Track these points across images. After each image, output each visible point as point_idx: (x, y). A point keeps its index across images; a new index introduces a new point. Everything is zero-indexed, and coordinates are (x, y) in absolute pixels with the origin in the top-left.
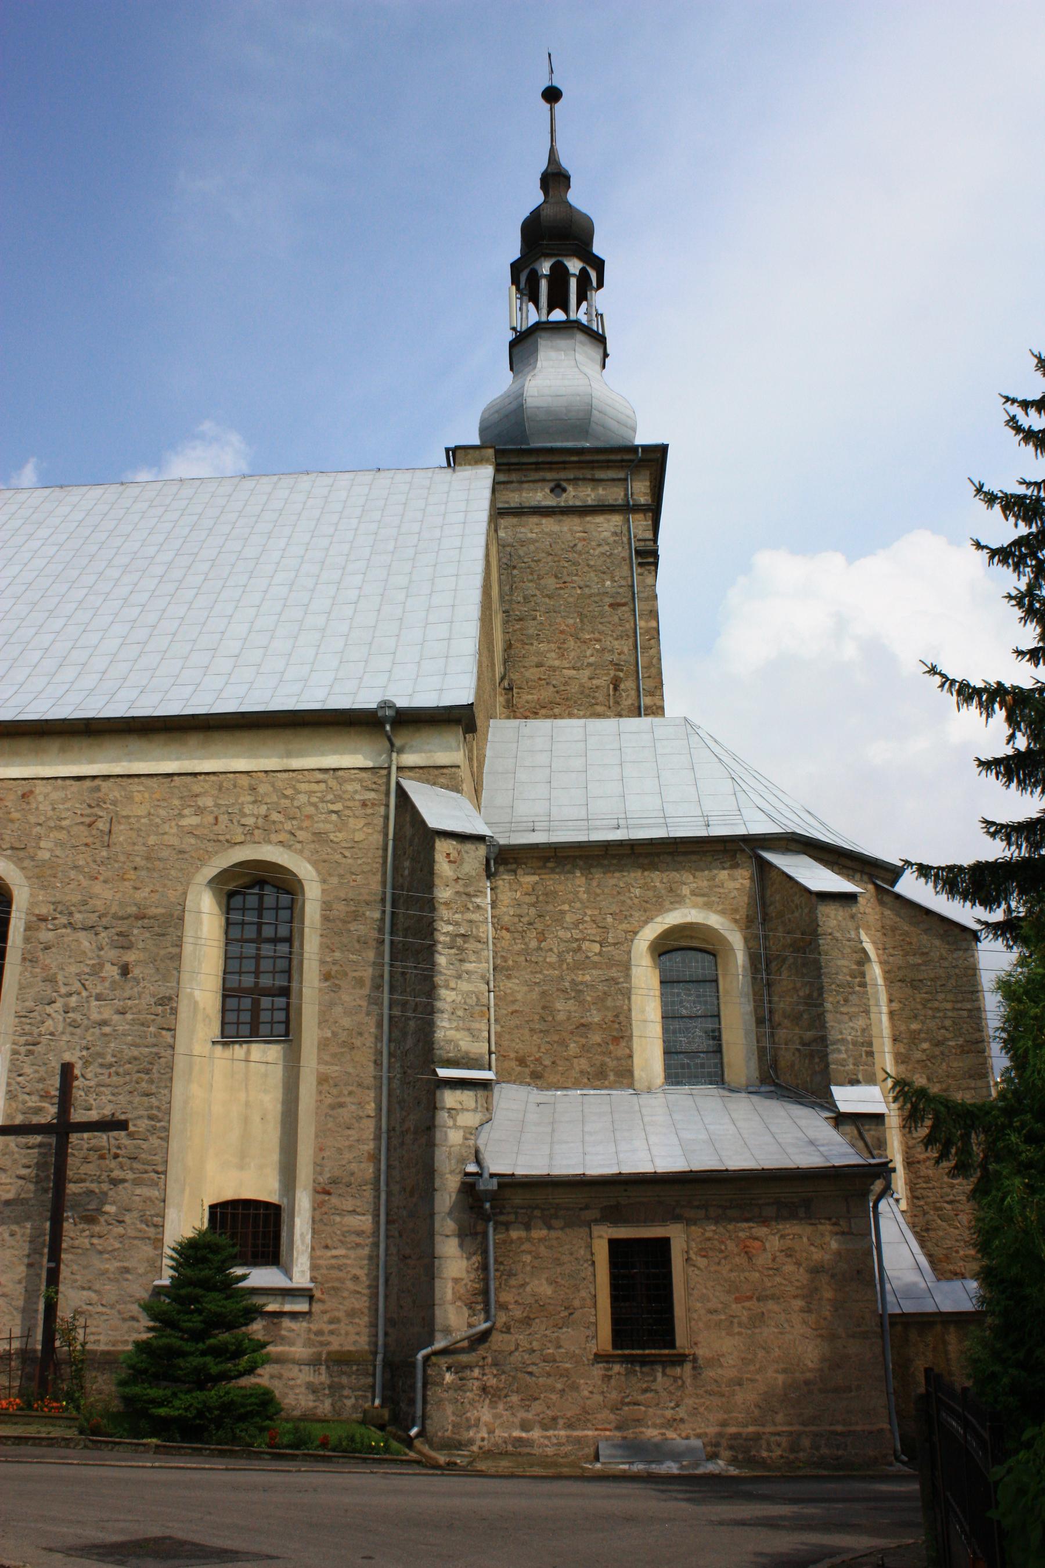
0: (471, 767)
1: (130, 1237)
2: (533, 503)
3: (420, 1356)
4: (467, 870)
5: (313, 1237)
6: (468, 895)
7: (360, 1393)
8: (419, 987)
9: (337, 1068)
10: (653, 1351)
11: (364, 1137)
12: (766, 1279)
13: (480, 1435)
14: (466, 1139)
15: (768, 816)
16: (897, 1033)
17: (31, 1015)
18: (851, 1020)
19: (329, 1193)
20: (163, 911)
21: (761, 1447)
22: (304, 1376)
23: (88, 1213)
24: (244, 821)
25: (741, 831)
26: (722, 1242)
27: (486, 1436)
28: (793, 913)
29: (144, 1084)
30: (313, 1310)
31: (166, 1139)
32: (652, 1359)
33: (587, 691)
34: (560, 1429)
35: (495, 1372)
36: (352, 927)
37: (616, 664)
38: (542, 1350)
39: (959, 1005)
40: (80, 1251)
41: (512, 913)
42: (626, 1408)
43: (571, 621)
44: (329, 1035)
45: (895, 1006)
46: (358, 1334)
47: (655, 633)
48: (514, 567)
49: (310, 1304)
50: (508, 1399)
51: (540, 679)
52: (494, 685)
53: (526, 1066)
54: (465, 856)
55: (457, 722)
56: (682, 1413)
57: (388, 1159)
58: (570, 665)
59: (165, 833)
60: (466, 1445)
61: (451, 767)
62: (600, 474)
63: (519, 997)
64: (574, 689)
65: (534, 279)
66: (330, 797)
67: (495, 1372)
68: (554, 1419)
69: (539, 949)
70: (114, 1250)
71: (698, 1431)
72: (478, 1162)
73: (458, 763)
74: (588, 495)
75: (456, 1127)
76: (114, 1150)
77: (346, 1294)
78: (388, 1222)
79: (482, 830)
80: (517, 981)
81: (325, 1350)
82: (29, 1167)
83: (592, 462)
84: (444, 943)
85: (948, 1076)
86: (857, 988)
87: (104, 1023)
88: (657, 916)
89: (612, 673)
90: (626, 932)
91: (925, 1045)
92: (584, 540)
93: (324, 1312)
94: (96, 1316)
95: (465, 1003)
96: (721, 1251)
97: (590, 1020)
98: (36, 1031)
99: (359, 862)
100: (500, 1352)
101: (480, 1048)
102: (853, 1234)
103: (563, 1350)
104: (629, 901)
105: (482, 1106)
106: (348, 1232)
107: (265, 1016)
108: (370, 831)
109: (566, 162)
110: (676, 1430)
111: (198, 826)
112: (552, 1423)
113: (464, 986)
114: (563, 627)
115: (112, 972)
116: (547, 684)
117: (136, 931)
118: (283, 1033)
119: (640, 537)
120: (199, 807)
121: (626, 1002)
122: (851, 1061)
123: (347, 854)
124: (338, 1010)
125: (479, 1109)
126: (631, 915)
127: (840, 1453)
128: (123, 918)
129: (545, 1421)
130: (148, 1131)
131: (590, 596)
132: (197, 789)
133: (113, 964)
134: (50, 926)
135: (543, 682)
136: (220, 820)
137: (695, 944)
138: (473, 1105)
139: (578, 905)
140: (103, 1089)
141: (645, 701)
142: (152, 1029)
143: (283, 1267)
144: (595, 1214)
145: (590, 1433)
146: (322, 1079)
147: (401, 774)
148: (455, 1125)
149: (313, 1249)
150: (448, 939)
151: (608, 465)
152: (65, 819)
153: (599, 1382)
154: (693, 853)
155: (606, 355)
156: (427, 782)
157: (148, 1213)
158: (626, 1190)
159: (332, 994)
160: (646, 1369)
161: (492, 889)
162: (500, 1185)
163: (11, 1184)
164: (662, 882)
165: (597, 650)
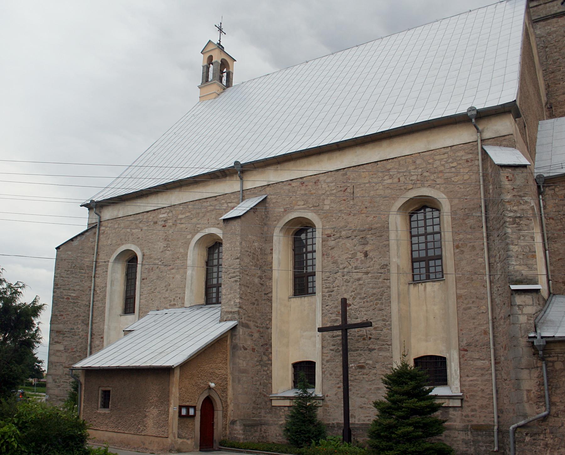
1: (379, 374)
2: (553, 13)
3: (511, 428)
5: (460, 372)
6: (520, 196)
7: (488, 444)
8: (500, 246)
9: (466, 290)
11: (482, 323)
17: (329, 279)
19: (466, 351)
20: (380, 225)
22: (461, 436)
23: (360, 364)
24: (412, 178)
29: (379, 305)
30: (463, 406)
31: (391, 329)
35: (552, 437)
36: (467, 222)
40: (358, 381)
41: (554, 210)
46: (485, 417)
48: (547, 47)
49: (462, 403)
52: (542, 105)
54: (516, 176)
55: (509, 112)
59: (377, 189)
61: (508, 135)
63: (561, 252)
66: (450, 160)
67: (552, 437)
70: (373, 380)
76: (369, 336)
78: (496, 363)
80: (560, 244)
81: (470, 424)
82: (335, 345)
84: (509, 222)
87: (359, 279)
93: (469, 406)
94: (368, 409)
95: (523, 251)
98: (332, 286)
99: (468, 189)
100: (553, 427)
106: (477, 368)
107: (432, 270)
108: (471, 174)
115: (360, 256)
117: (368, 236)
118: (441, 277)
123: (462, 187)
124: (464, 263)
125: (535, 305)
128: (362, 231)
130: (383, 326)
132: (389, 167)
133: (361, 252)
134: (332, 239)
136: (401, 179)
138: (531, 303)
140: (362, 309)
142: (380, 280)
146: (459, 297)
147: (483, 143)
148: (522, 313)
149: (461, 377)
150: (511, 220)
152: (333, 190)
156: (497, 145)
157: (386, 363)
159: (460, 255)
161: (543, 200)
162: (547, 342)
163: (327, 353)
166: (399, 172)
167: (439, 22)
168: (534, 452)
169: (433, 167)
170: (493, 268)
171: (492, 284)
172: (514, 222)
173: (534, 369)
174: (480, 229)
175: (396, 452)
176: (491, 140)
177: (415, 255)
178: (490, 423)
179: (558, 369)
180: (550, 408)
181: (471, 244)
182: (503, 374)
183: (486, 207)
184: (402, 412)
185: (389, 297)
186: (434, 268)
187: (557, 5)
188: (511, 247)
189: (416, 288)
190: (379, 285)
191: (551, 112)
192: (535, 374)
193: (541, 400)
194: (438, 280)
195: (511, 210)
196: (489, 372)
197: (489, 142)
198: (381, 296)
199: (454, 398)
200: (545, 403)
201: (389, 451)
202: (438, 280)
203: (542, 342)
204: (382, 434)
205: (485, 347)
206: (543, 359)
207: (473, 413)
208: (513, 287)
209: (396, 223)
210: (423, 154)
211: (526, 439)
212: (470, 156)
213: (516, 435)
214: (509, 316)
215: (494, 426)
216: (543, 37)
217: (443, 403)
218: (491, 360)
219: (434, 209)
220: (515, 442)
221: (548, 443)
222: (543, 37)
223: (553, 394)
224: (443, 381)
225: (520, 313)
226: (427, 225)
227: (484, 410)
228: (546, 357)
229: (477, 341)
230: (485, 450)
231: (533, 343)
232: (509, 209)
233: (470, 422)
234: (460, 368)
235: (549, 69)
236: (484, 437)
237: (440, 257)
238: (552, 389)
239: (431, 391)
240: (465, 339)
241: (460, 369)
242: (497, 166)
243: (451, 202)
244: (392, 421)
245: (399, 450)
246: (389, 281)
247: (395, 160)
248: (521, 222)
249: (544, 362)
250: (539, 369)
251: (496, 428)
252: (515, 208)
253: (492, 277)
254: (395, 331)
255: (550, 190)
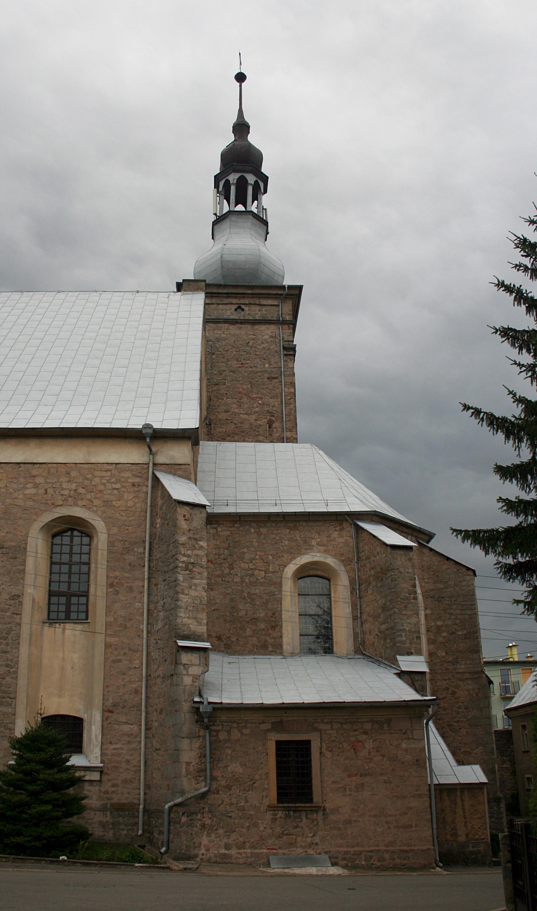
0: (194, 465)
2: (225, 317)
3: (167, 807)
4: (195, 525)
5: (102, 737)
6: (196, 539)
7: (130, 827)
9: (117, 639)
10: (301, 805)
12: (365, 764)
13: (201, 852)
14: (193, 681)
15: (361, 501)
16: (429, 627)
18: (408, 618)
19: (112, 712)
20: (15, 544)
21: (361, 858)
22: (98, 817)
24: (63, 492)
25: (347, 509)
26: (341, 743)
27: (205, 852)
28: (375, 557)
30: (103, 779)
32: (300, 809)
33: (254, 428)
34: (247, 849)
35: (210, 816)
36: (126, 557)
37: (271, 413)
38: (237, 804)
39: (463, 612)
41: (214, 553)
42: (285, 837)
43: (245, 387)
44: (112, 620)
45: (428, 612)
46: (128, 793)
47: (293, 395)
48: (213, 354)
50: (218, 831)
51: (227, 419)
53: (222, 641)
54: (194, 517)
56: (317, 839)
57: (146, 693)
58: (244, 412)
59: (16, 498)
60: (193, 858)
61: (185, 464)
62: (264, 302)
63: (218, 601)
64: (246, 426)
65: (227, 185)
67: (210, 816)
68: (244, 843)
69: (230, 574)
71: (326, 850)
72: (200, 696)
73: (189, 463)
74: (255, 312)
75: (188, 674)
77: (121, 770)
78: (146, 729)
79: (203, 501)
80: (217, 592)
83: (260, 294)
84: (182, 567)
85: (457, 652)
86: (412, 601)
88: (297, 557)
89: (268, 417)
90: (280, 565)
91: (445, 634)
92: (254, 340)
93: (109, 780)
95: (193, 602)
96: (340, 748)
97: (258, 615)
99: (131, 519)
101: (203, 629)
102: (415, 739)
103: (249, 804)
104: (281, 548)
105: (203, 663)
107: (74, 608)
108: (137, 501)
109: (247, 118)
110: (313, 849)
111: (35, 494)
112: (241, 846)
113: (193, 593)
114: (241, 390)
116: (231, 422)
119: (286, 339)
120: (36, 483)
121: (279, 606)
122: (408, 641)
126: (283, 556)
127: (406, 862)
129: (239, 844)
130: (5, 673)
131: (257, 372)
132: (35, 472)
135: (229, 421)
136: (48, 491)
137: (319, 573)
139: (252, 549)
141: (289, 434)
142: (8, 614)
143: (84, 754)
144: (268, 726)
145: (264, 851)
146: (108, 646)
147: (155, 468)
149: (102, 744)
150: (184, 565)
151: (268, 296)
153: (270, 822)
154: (318, 521)
155: (267, 233)
156: (170, 473)
157: (5, 722)
158: (286, 713)
160: (297, 814)
162: (214, 709)
164: (300, 537)
165: (260, 404)
166: (46, 483)
167: (98, 294)
168: (190, 834)
169: (91, 484)
170: (152, 616)
171: (149, 635)
172: (186, 569)
173: (195, 739)
174: (141, 568)
175: (26, 839)
176: (164, 466)
177: (55, 588)
178: (134, 801)
179: (222, 739)
180: (210, 784)
181: (128, 585)
182: (154, 742)
183: (150, 543)
184: (37, 786)
185: (18, 636)
186: (77, 606)
187: (230, 309)
188: (181, 596)
189: (52, 629)
190: (6, 620)
191: (210, 429)
192: (196, 744)
193: (201, 774)
194: (81, 623)
195: (184, 554)
196: (138, 739)
197: (161, 468)
198: (7, 634)
199: (92, 769)
200: (205, 778)
201: (16, 837)
202: (81, 623)
203: (209, 709)
204: (9, 813)
205: (135, 708)
206: (207, 728)
207: (113, 789)
208: (181, 643)
209: (37, 545)
210: (80, 465)
211: (183, 819)
212: (138, 480)
213: (172, 815)
214: (172, 675)
215: (139, 804)
216: (211, 341)
217: (84, 776)
218: (141, 725)
219: (85, 534)
220: (169, 824)
221: (206, 823)
222: (211, 341)
223: (215, 766)
224: (78, 749)
225: (185, 673)
226: (74, 552)
227: (128, 786)
228: (211, 726)
229: (126, 701)
230: (126, 835)
231: (198, 709)
232: (183, 553)
233: (110, 799)
234: (102, 732)
235: (213, 379)
236: (126, 818)
237: (86, 594)
238: (214, 761)
239: (68, 760)
240: (111, 698)
241: (103, 735)
242: (174, 502)
243: (109, 530)
244: (23, 797)
245: (31, 836)
246: (19, 616)
247: (43, 465)
248: (194, 569)
249: (207, 731)
250: (201, 739)
251: (141, 807)
252: (189, 552)
253: (149, 626)
254: (22, 682)
255: (212, 528)
